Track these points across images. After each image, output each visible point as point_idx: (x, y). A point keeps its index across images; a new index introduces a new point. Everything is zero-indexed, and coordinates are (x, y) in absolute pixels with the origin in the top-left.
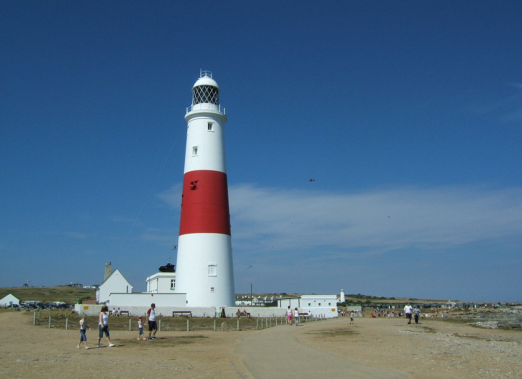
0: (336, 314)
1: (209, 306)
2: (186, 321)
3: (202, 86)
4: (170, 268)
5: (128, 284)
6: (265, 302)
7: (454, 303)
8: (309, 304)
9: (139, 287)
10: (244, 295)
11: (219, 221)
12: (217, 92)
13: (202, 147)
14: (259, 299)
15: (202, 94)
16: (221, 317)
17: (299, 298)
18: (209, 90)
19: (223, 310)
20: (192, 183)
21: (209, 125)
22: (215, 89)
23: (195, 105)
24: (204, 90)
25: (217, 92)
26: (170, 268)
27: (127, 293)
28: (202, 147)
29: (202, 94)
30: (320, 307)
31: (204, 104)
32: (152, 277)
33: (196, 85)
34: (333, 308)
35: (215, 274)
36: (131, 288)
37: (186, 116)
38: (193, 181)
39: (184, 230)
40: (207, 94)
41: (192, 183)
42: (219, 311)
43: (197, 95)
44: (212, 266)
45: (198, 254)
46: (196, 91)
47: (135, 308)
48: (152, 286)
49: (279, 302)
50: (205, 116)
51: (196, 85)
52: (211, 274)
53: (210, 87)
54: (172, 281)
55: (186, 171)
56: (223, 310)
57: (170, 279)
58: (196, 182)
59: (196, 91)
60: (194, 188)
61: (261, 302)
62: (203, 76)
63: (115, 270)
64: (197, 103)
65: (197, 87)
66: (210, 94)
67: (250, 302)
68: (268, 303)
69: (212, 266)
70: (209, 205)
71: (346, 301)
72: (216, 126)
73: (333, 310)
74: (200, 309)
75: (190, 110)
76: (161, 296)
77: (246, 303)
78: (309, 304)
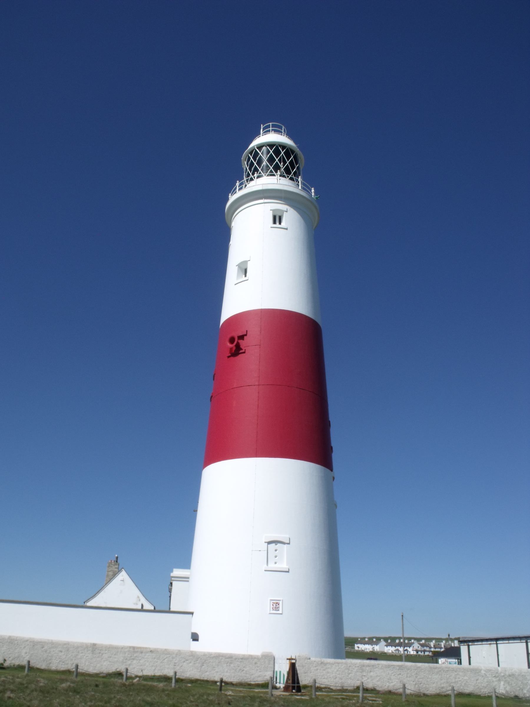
1: (256, 652)
6: (432, 650)
9: (398, 650)
13: (264, 261)
14: (422, 645)
16: (286, 689)
18: (277, 152)
19: (293, 667)
20: (232, 340)
21: (274, 218)
22: (289, 152)
28: (264, 261)
35: (284, 566)
38: (236, 334)
39: (217, 451)
44: (276, 542)
45: (251, 512)
52: (272, 566)
58: (242, 337)
61: (425, 648)
63: (120, 571)
64: (252, 179)
65: (260, 147)
66: (284, 161)
68: (437, 652)
69: (276, 542)
72: (291, 217)
74: (230, 659)
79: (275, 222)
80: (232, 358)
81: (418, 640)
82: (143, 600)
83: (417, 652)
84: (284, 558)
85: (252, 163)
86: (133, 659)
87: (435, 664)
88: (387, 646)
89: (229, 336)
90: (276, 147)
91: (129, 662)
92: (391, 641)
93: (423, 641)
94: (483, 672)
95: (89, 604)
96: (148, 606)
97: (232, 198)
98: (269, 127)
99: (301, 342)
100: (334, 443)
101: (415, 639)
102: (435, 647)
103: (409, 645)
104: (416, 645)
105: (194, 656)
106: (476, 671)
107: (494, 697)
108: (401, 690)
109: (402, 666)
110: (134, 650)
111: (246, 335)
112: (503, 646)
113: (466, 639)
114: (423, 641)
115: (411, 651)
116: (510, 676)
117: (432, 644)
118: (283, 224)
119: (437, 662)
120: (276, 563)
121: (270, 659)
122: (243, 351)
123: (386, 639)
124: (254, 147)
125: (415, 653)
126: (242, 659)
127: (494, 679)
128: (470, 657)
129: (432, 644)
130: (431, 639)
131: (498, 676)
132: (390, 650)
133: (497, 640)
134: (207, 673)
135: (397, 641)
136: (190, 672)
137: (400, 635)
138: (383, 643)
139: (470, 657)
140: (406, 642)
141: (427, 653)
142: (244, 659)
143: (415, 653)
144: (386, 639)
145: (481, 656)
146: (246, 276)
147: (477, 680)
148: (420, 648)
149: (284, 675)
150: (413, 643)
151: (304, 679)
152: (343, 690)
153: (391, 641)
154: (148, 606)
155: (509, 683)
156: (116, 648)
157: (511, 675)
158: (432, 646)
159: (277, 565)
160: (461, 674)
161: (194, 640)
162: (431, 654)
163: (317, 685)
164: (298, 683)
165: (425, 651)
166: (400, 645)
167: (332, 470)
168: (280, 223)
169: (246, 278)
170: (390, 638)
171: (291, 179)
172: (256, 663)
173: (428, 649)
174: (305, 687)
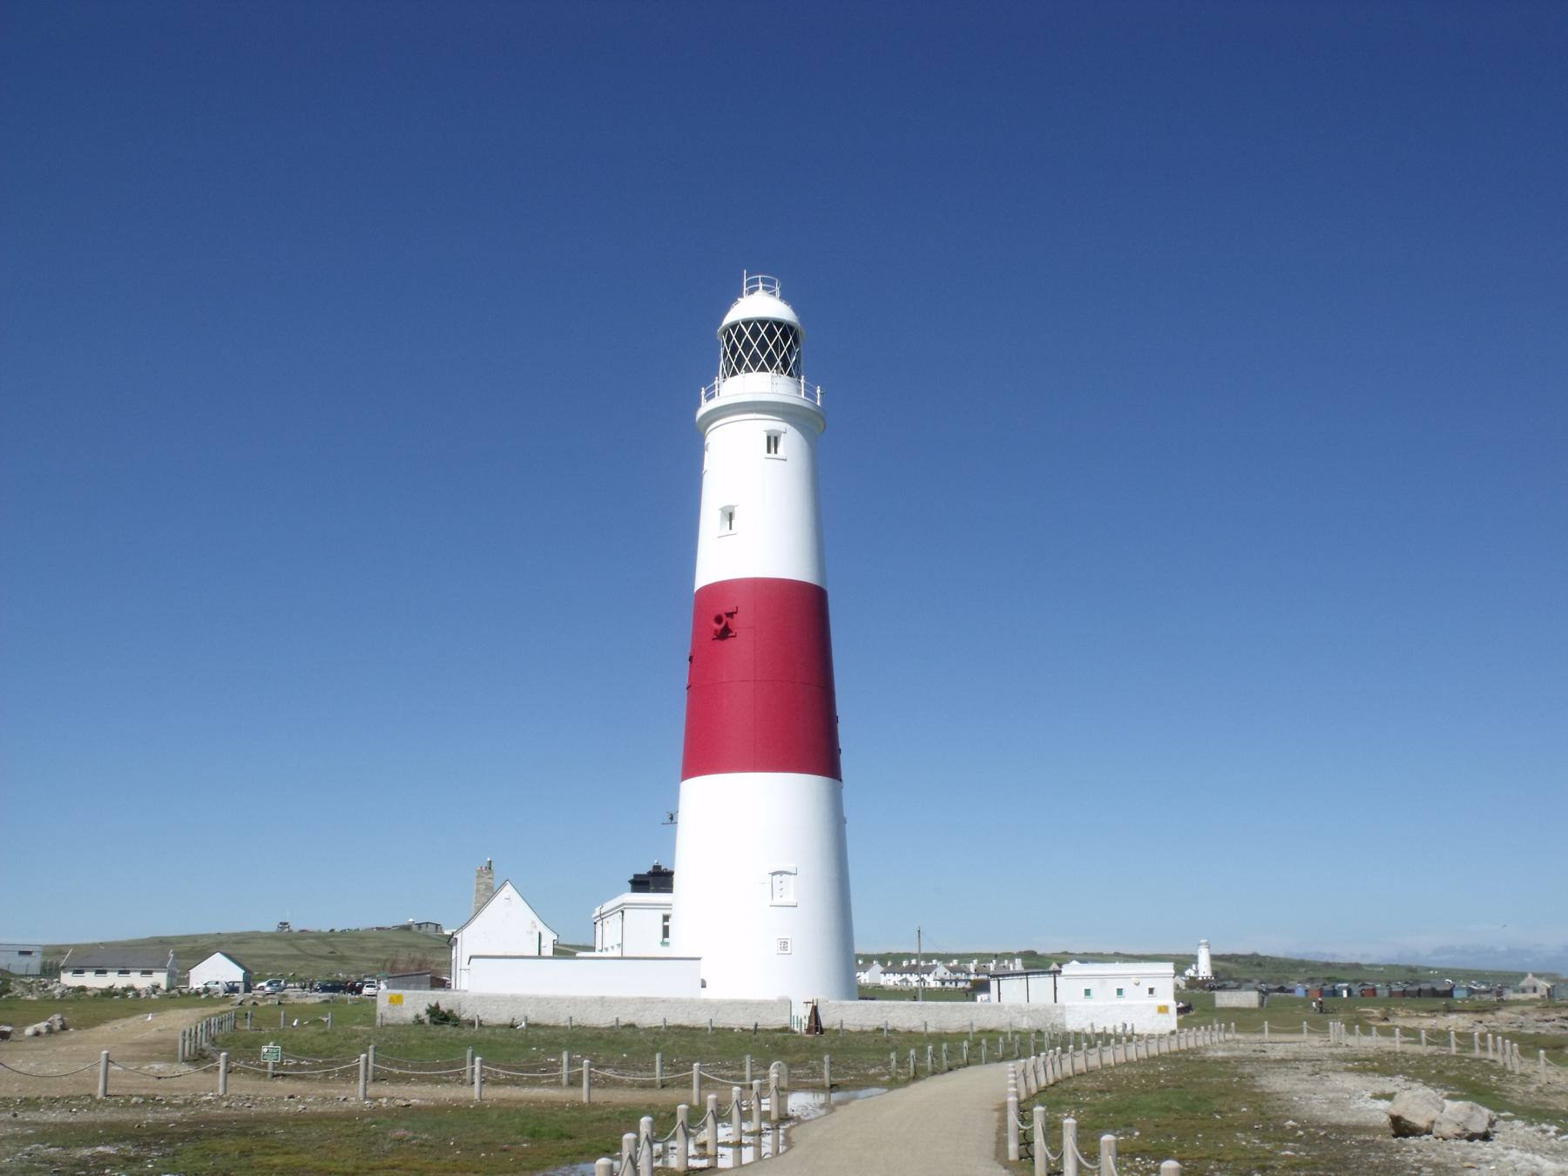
0: (1171, 1022)
2: (161, 967)
3: (747, 323)
4: (657, 880)
5: (541, 927)
6: (972, 977)
7: (1543, 985)
8: (1120, 992)
11: (806, 737)
12: (796, 340)
13: (751, 509)
14: (953, 970)
15: (747, 346)
16: (809, 1031)
18: (771, 334)
19: (815, 1009)
20: (719, 620)
21: (769, 439)
22: (787, 330)
23: (729, 379)
24: (755, 333)
25: (796, 340)
26: (657, 880)
27: (540, 957)
28: (751, 509)
29: (747, 346)
30: (1122, 1001)
32: (608, 906)
33: (729, 319)
34: (1163, 1002)
35: (791, 900)
36: (549, 938)
37: (701, 412)
38: (721, 610)
39: (700, 760)
41: (719, 620)
42: (802, 1013)
43: (734, 349)
45: (745, 829)
46: (729, 338)
47: (539, 1001)
48: (608, 934)
49: (993, 984)
50: (751, 412)
51: (729, 319)
53: (772, 325)
54: (666, 918)
56: (815, 1009)
57: (659, 914)
58: (730, 615)
59: (729, 338)
60: (724, 634)
62: (751, 292)
63: (504, 884)
64: (734, 373)
65: (734, 326)
66: (769, 345)
70: (776, 685)
71: (1215, 973)
72: (792, 440)
73: (1163, 1010)
75: (713, 396)
76: (639, 969)
78: (1087, 992)
80: (719, 642)
81: (945, 958)
84: (791, 891)
90: (755, 325)
92: (892, 962)
93: (955, 962)
97: (706, 407)
98: (756, 281)
99: (801, 615)
100: (842, 744)
103: (928, 970)
104: (941, 971)
105: (708, 1004)
110: (645, 1000)
115: (932, 982)
117: (972, 967)
119: (974, 999)
123: (882, 959)
125: (939, 985)
129: (972, 967)
130: (968, 957)
132: (891, 980)
135: (905, 963)
136: (701, 1019)
138: (877, 967)
140: (922, 962)
141: (961, 985)
142: (760, 1004)
143: (939, 985)
148: (947, 977)
151: (825, 1023)
152: (863, 1033)
153: (892, 962)
156: (626, 1000)
162: (968, 986)
165: (957, 981)
166: (912, 970)
171: (790, 375)
173: (963, 976)
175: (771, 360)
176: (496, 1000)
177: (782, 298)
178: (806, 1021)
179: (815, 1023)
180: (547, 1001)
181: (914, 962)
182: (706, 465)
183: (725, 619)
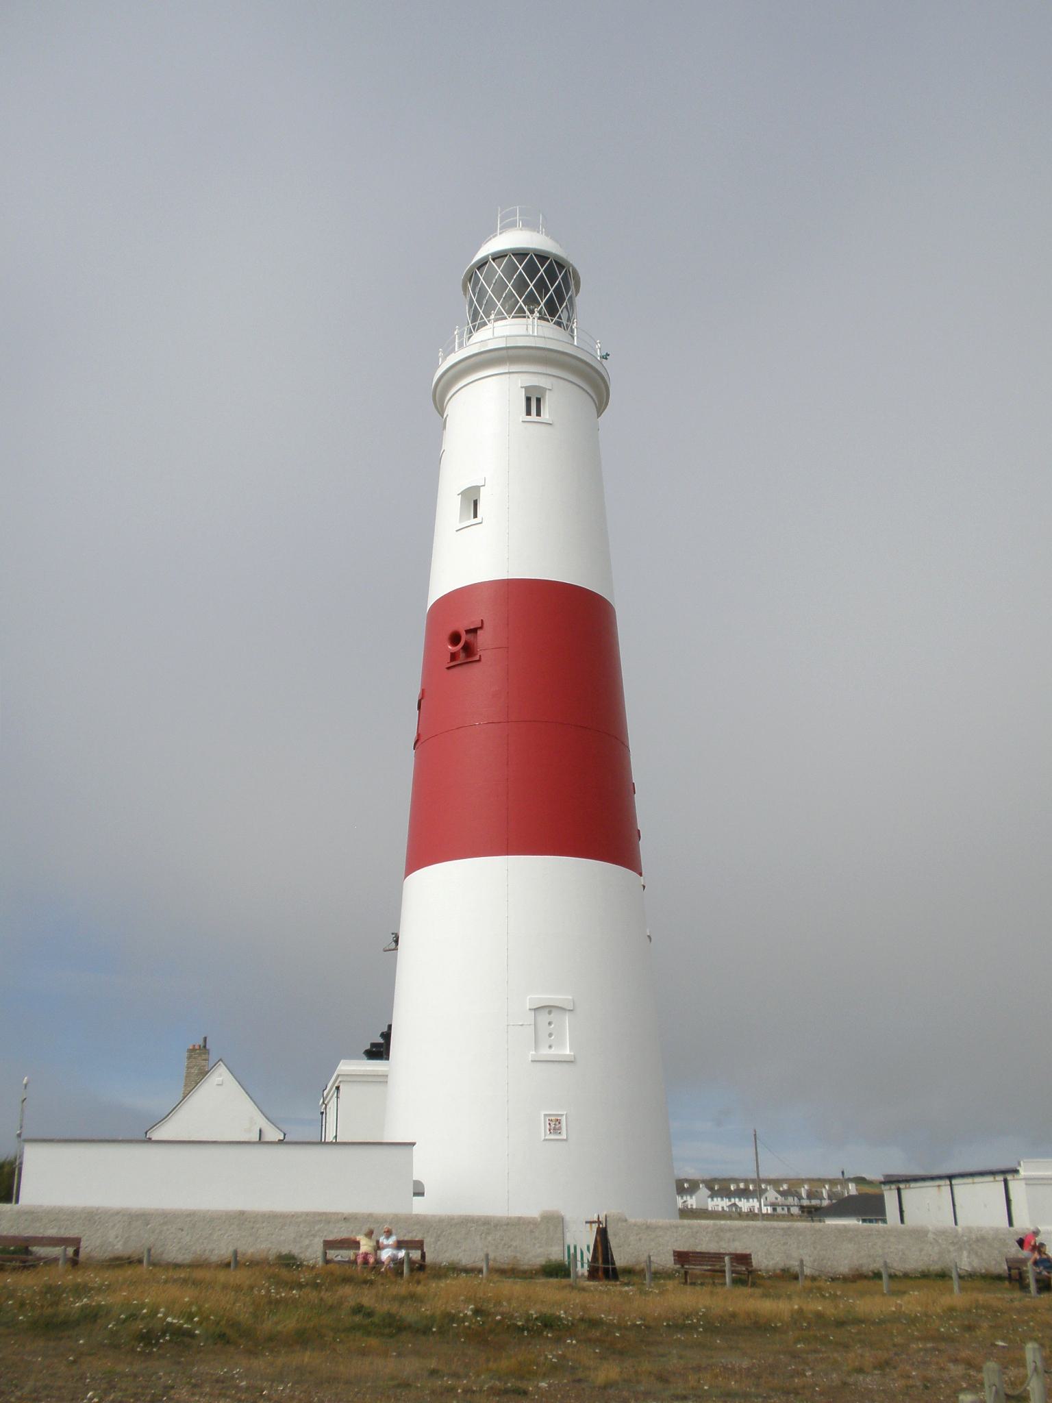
1: (532, 1211)
6: (805, 1202)
9: (735, 1204)
10: (736, 1181)
14: (783, 1194)
17: (1007, 1173)
19: (602, 1234)
21: (528, 400)
31: (510, 321)
38: (462, 626)
39: (427, 847)
40: (521, 286)
41: (455, 638)
42: (583, 1240)
52: (545, 1052)
55: (440, 587)
61: (790, 1200)
67: (753, 1203)
69: (550, 1009)
74: (487, 1225)
77: (745, 1205)
79: (529, 413)
81: (775, 1183)
82: (262, 1122)
83: (775, 1210)
85: (482, 288)
86: (314, 1236)
87: (881, 1225)
88: (712, 1197)
89: (450, 629)
91: (307, 1242)
92: (720, 1187)
94: (930, 1236)
95: (156, 1135)
96: (273, 1134)
98: (513, 213)
101: (769, 1182)
102: (810, 1196)
104: (772, 1195)
106: (919, 1234)
107: (954, 1275)
108: (797, 1269)
109: (789, 1228)
111: (481, 628)
112: (963, 1188)
113: (970, 1180)
114: (785, 1187)
116: (977, 1240)
118: (546, 415)
120: (550, 1047)
121: (554, 1223)
122: (477, 658)
123: (709, 1184)
124: (487, 257)
126: (508, 1224)
127: (952, 1248)
128: (901, 1212)
131: (958, 1240)
133: (950, 1177)
134: (447, 1255)
137: (754, 1176)
138: (703, 1191)
139: (901, 1212)
144: (709, 1184)
145: (926, 1207)
146: (475, 516)
147: (921, 1250)
149: (110, 1288)
150: (766, 1190)
151: (621, 1258)
153: (720, 1187)
154: (273, 1134)
155: (976, 1253)
157: (981, 1240)
158: (804, 1195)
159: (553, 1051)
160: (892, 1239)
161: (416, 1194)
163: (654, 1267)
164: (613, 1263)
167: (641, 874)
168: (538, 414)
169: (476, 521)
170: (715, 1180)
171: (559, 324)
172: (532, 1232)
174: (629, 1271)
175: (531, 301)
176: (192, 1220)
177: (547, 235)
178: (588, 1256)
179: (604, 1265)
180: (167, 1218)
181: (742, 1186)
182: (446, 446)
183: (464, 638)
